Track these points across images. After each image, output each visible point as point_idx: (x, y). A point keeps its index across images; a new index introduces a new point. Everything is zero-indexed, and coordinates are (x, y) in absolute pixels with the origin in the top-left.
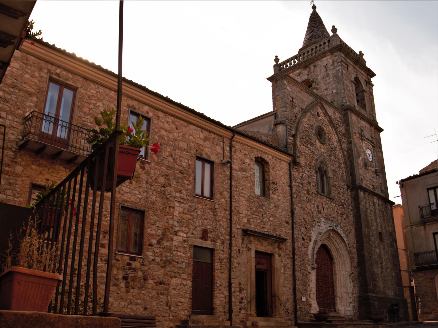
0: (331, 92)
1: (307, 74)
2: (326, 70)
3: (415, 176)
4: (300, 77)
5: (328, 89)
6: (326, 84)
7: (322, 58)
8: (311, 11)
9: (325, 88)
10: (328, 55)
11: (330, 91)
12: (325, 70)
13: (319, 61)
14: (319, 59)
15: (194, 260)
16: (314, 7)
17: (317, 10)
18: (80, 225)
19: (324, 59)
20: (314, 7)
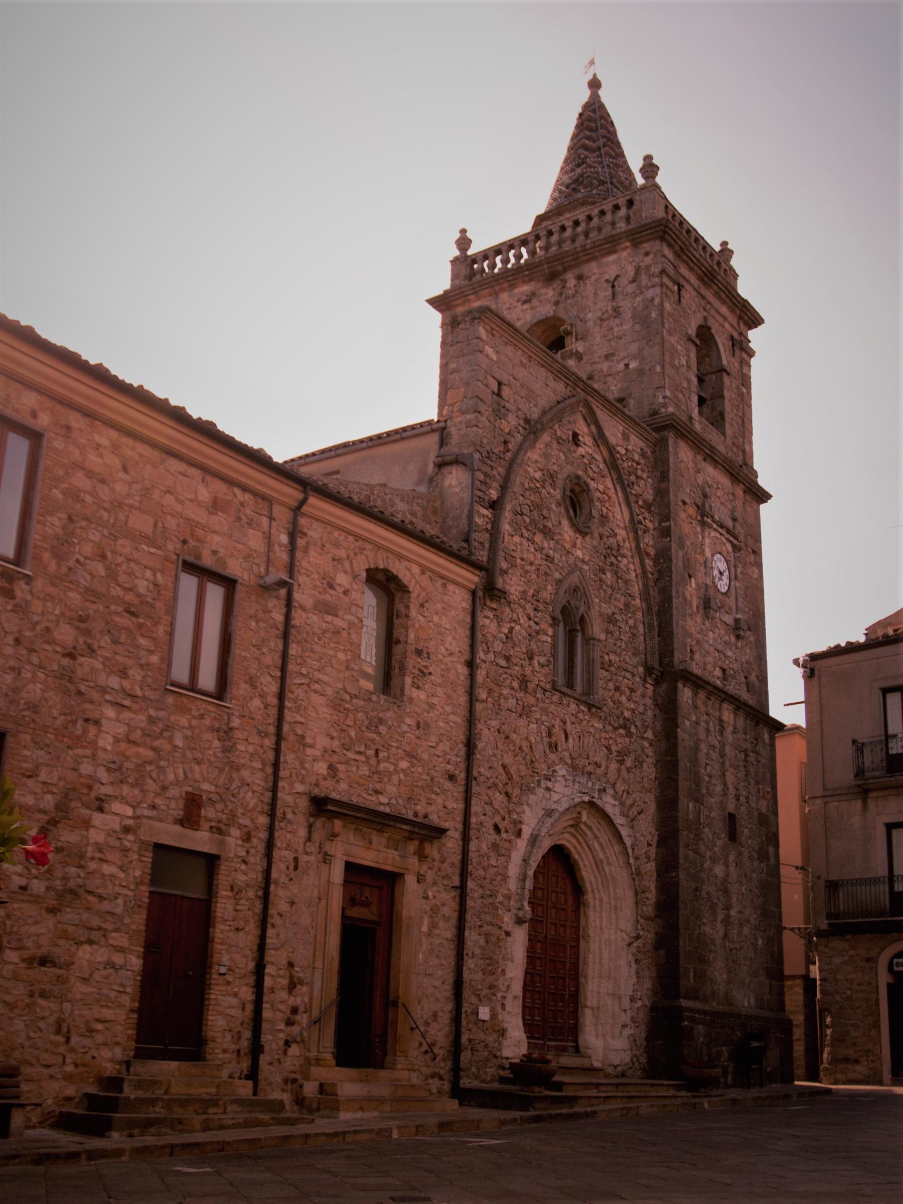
0: (621, 366)
1: (553, 299)
2: (614, 294)
3: (852, 648)
4: (532, 308)
5: (612, 355)
8: (585, 95)
9: (604, 351)
10: (622, 246)
11: (618, 362)
13: (594, 264)
16: (595, 84)
17: (601, 92)
19: (612, 258)
20: (595, 84)
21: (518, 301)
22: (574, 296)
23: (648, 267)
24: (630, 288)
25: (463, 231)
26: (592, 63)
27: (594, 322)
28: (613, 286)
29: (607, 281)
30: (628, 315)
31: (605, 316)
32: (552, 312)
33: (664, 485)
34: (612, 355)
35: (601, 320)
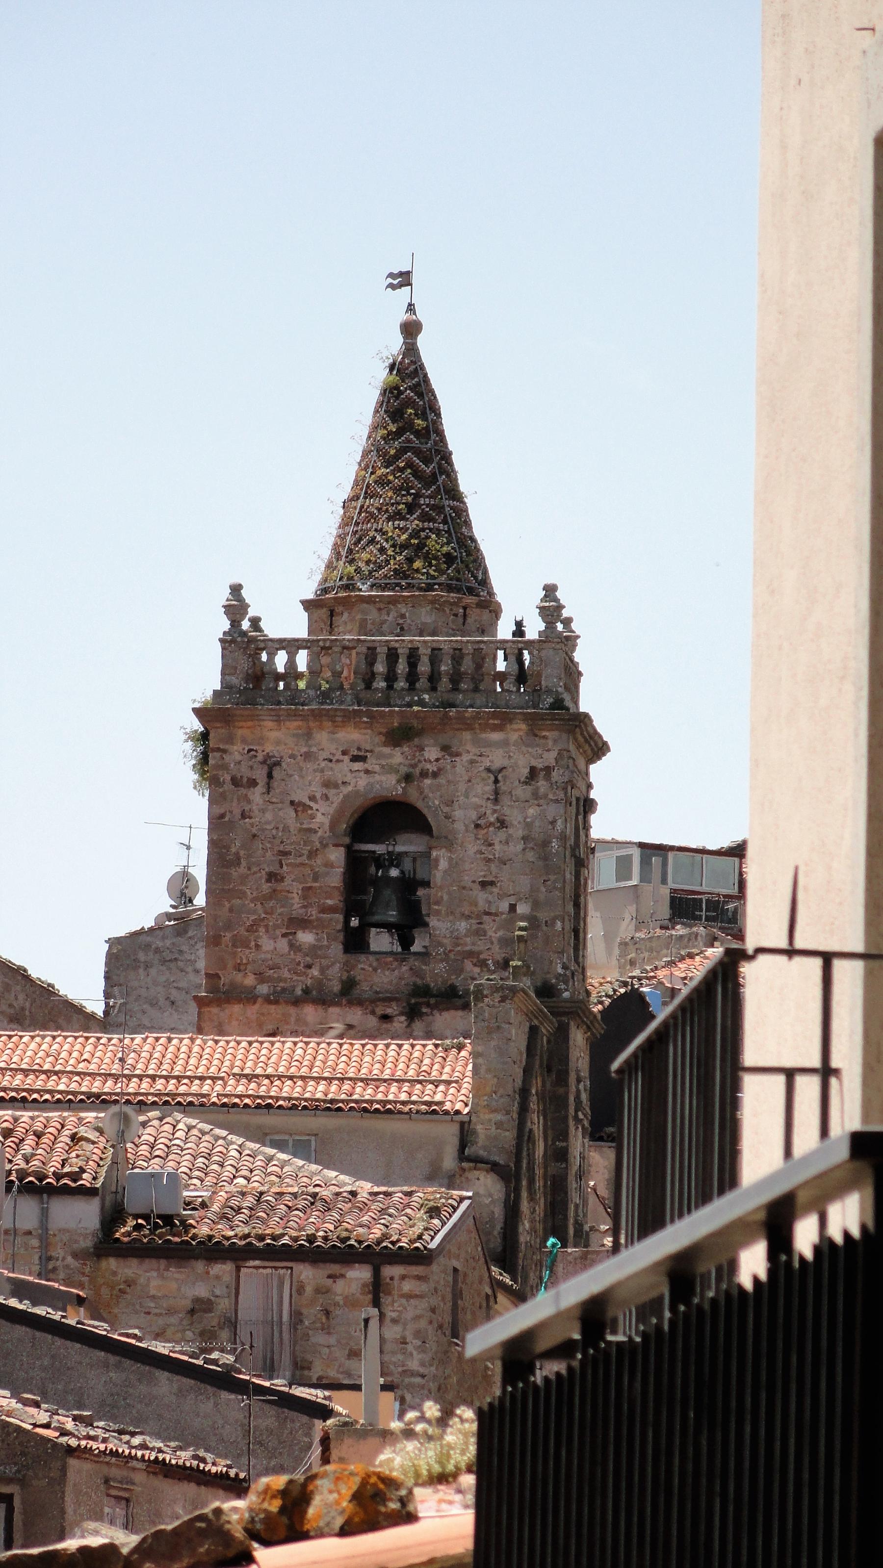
0: (504, 906)
1: (404, 770)
2: (497, 792)
3: (27, 978)
4: (367, 772)
5: (492, 883)
6: (489, 860)
7: (485, 727)
8: (396, 343)
9: (480, 875)
10: (515, 726)
11: (501, 897)
12: (490, 788)
13: (467, 736)
14: (469, 727)
15: (396, 1416)
16: (411, 330)
17: (422, 342)
18: (763, 1395)
19: (496, 736)
20: (411, 330)
21: (344, 753)
22: (435, 775)
23: (548, 770)
24: (522, 792)
25: (236, 589)
26: (404, 279)
27: (466, 826)
28: (496, 781)
29: (488, 770)
30: (518, 832)
31: (481, 822)
32: (400, 791)
33: (561, 1090)
34: (492, 883)
35: (477, 826)
